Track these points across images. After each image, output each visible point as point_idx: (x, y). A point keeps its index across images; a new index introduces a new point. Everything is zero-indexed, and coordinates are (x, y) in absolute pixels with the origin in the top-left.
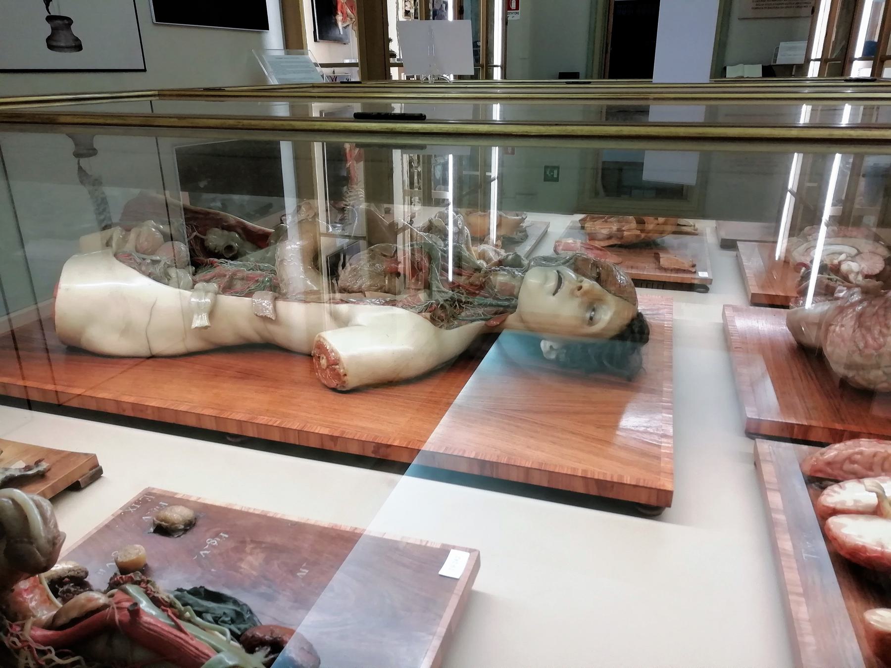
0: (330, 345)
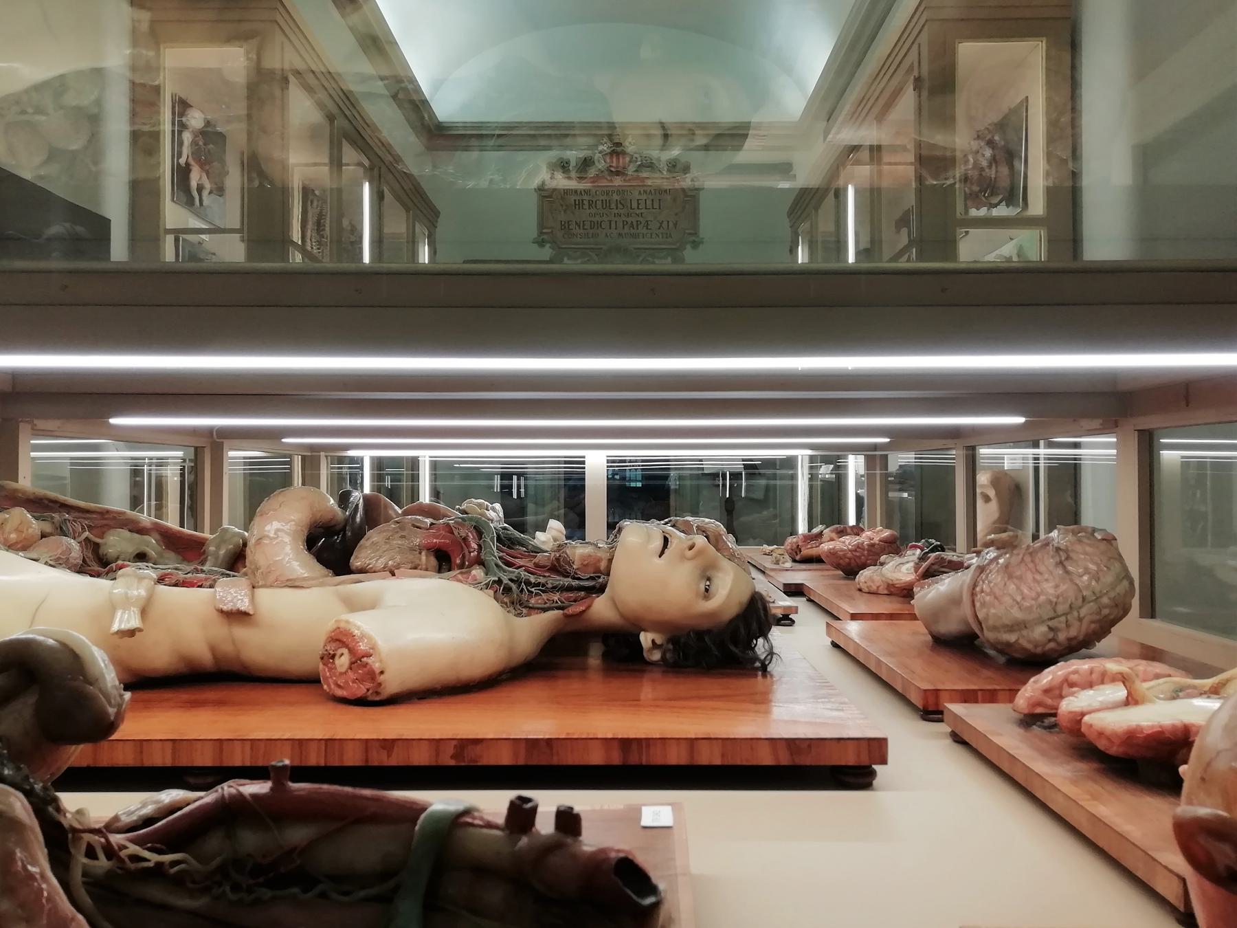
0: (358, 628)
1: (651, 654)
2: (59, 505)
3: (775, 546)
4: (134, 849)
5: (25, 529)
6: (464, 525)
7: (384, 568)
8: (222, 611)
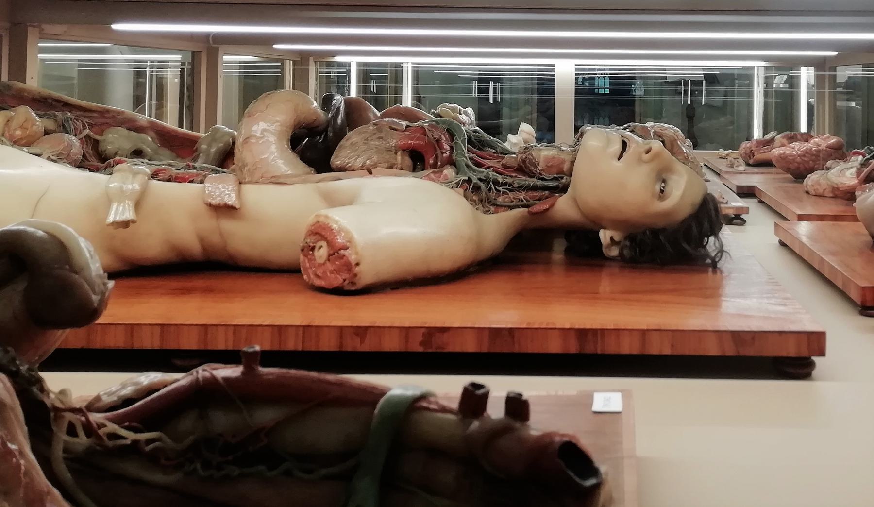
0: (337, 222)
1: (610, 250)
2: (62, 104)
3: (731, 150)
4: (112, 427)
5: (29, 126)
6: (438, 128)
7: (362, 166)
8: (210, 205)
